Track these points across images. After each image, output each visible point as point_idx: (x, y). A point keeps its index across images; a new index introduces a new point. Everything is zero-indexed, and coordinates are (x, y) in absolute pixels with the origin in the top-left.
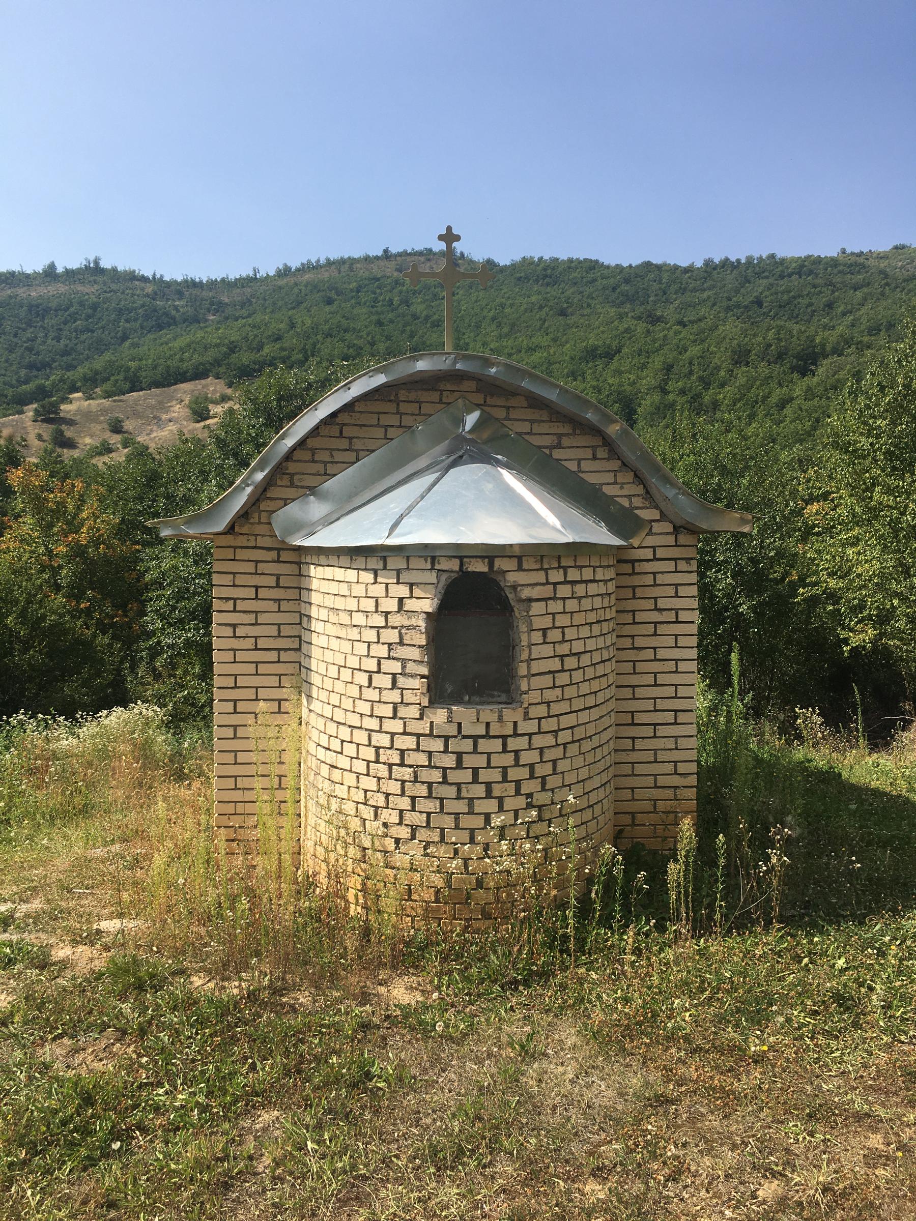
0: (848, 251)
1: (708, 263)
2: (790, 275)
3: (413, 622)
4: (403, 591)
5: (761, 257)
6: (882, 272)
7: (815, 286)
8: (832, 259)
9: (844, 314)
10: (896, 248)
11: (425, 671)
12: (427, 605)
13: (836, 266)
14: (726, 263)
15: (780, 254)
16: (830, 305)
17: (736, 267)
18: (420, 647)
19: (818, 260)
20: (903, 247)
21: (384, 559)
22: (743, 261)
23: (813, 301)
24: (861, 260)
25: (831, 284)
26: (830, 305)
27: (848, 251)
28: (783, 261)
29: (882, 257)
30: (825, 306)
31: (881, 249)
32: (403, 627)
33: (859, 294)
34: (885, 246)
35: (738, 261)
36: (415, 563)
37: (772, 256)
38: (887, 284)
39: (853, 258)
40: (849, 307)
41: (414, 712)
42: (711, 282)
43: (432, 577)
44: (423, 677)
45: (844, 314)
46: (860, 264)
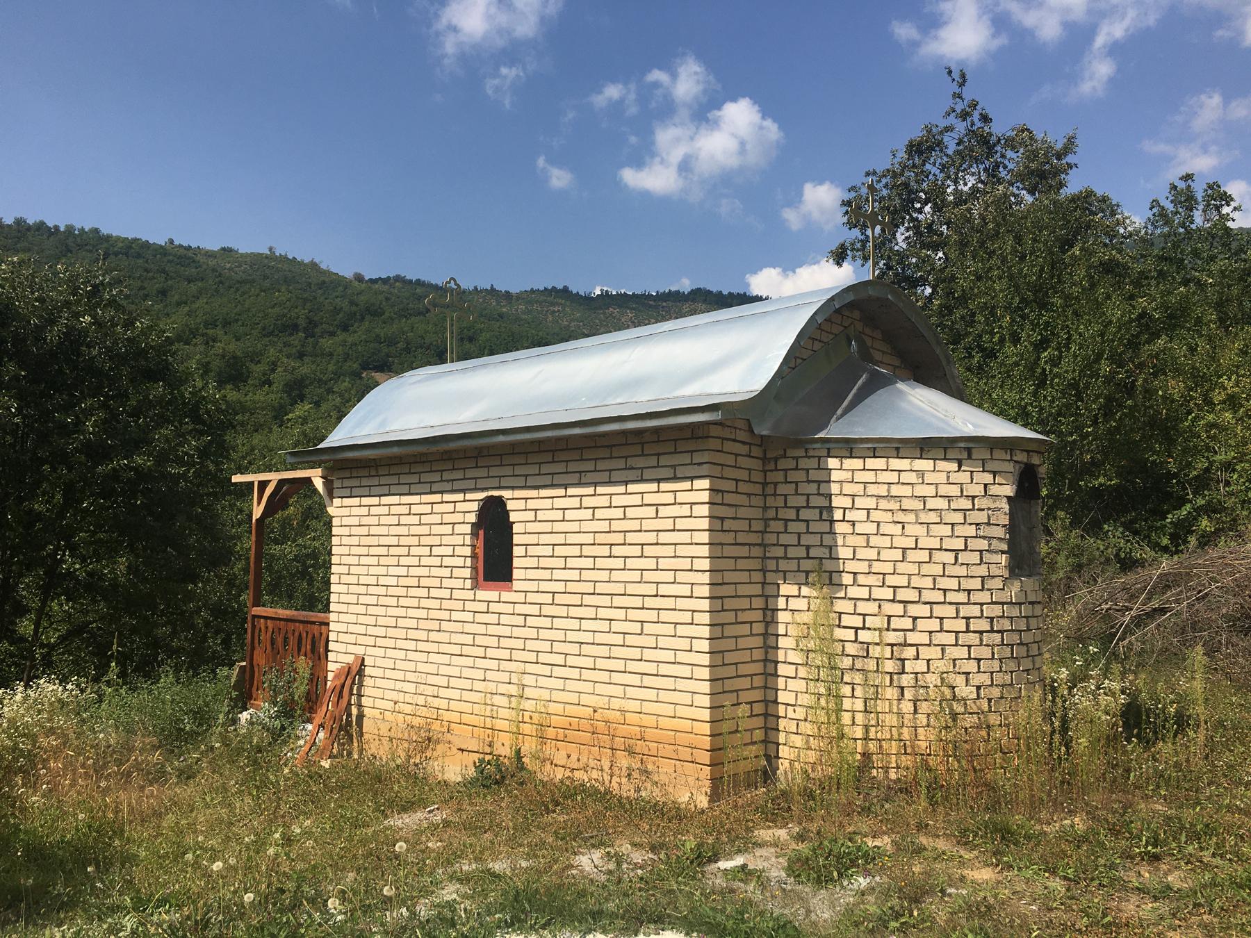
0: (177, 243)
1: (19, 222)
2: (116, 254)
3: (998, 504)
4: (988, 478)
5: (83, 229)
6: (214, 270)
7: (146, 270)
8: (161, 246)
9: (178, 304)
10: (223, 249)
11: (1005, 547)
12: (1009, 490)
13: (165, 255)
14: (41, 226)
15: (105, 231)
16: (163, 293)
17: (53, 233)
18: (1004, 526)
19: (146, 245)
20: (230, 250)
21: (969, 450)
22: (62, 229)
23: (146, 285)
24: (190, 254)
25: (164, 271)
26: (163, 293)
27: (177, 243)
28: (108, 238)
29: (210, 254)
30: (159, 292)
31: (209, 247)
32: (989, 509)
33: (193, 288)
34: (214, 246)
35: (57, 228)
36: (999, 454)
37: (96, 231)
38: (221, 282)
39: (182, 250)
40: (184, 298)
41: (998, 583)
42: (26, 244)
43: (1009, 467)
44: (1003, 552)
45: (178, 304)
46: (190, 258)
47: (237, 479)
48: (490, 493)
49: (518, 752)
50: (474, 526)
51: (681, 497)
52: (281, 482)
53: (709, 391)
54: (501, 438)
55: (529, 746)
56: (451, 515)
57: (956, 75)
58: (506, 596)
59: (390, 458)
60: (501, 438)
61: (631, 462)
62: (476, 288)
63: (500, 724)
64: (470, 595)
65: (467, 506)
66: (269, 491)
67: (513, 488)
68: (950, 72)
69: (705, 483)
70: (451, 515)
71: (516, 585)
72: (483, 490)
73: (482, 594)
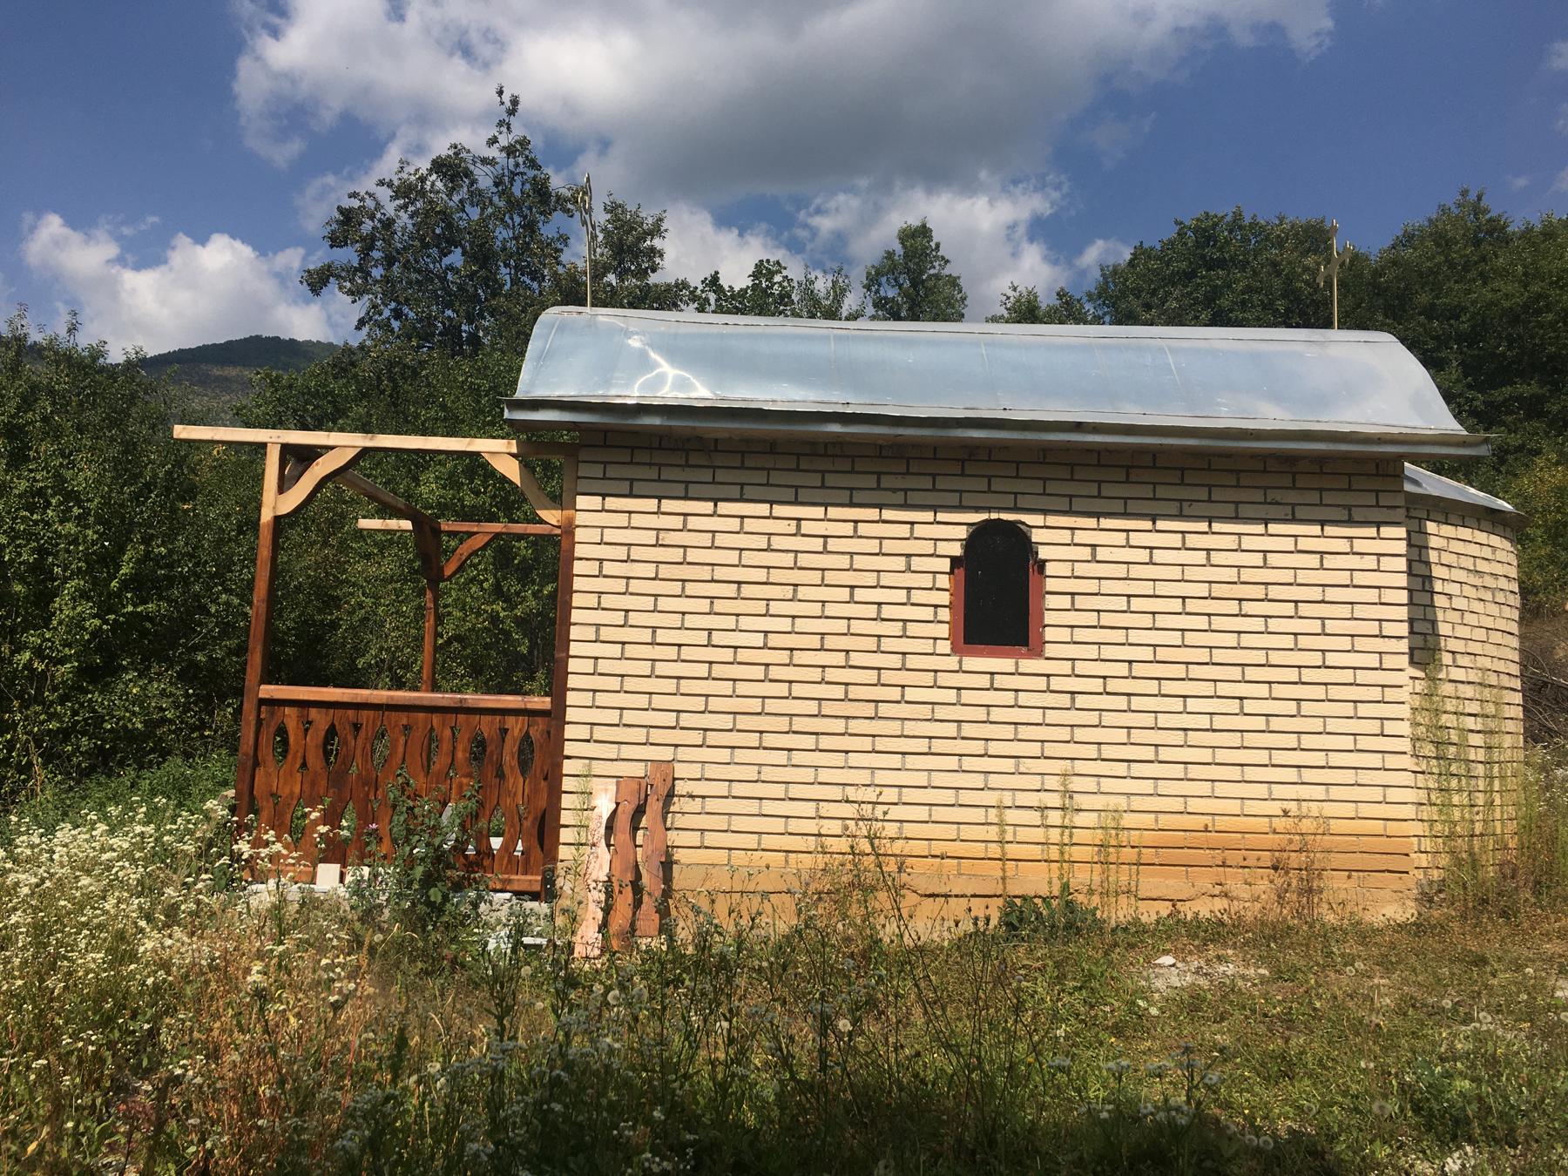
47: (181, 432)
48: (994, 516)
49: (1065, 887)
50: (955, 561)
51: (1192, 540)
52: (365, 452)
53: (1373, 420)
54: (835, 428)
55: (1081, 877)
56: (922, 546)
57: (506, 98)
58: (1028, 665)
59: (748, 441)
60: (835, 428)
61: (1272, 495)
62: (1238, 216)
63: (1077, 853)
64: (953, 662)
65: (949, 532)
66: (322, 468)
67: (1045, 512)
68: (500, 93)
69: (1401, 532)
70: (922, 546)
71: (1050, 650)
72: (977, 509)
73: (971, 663)
